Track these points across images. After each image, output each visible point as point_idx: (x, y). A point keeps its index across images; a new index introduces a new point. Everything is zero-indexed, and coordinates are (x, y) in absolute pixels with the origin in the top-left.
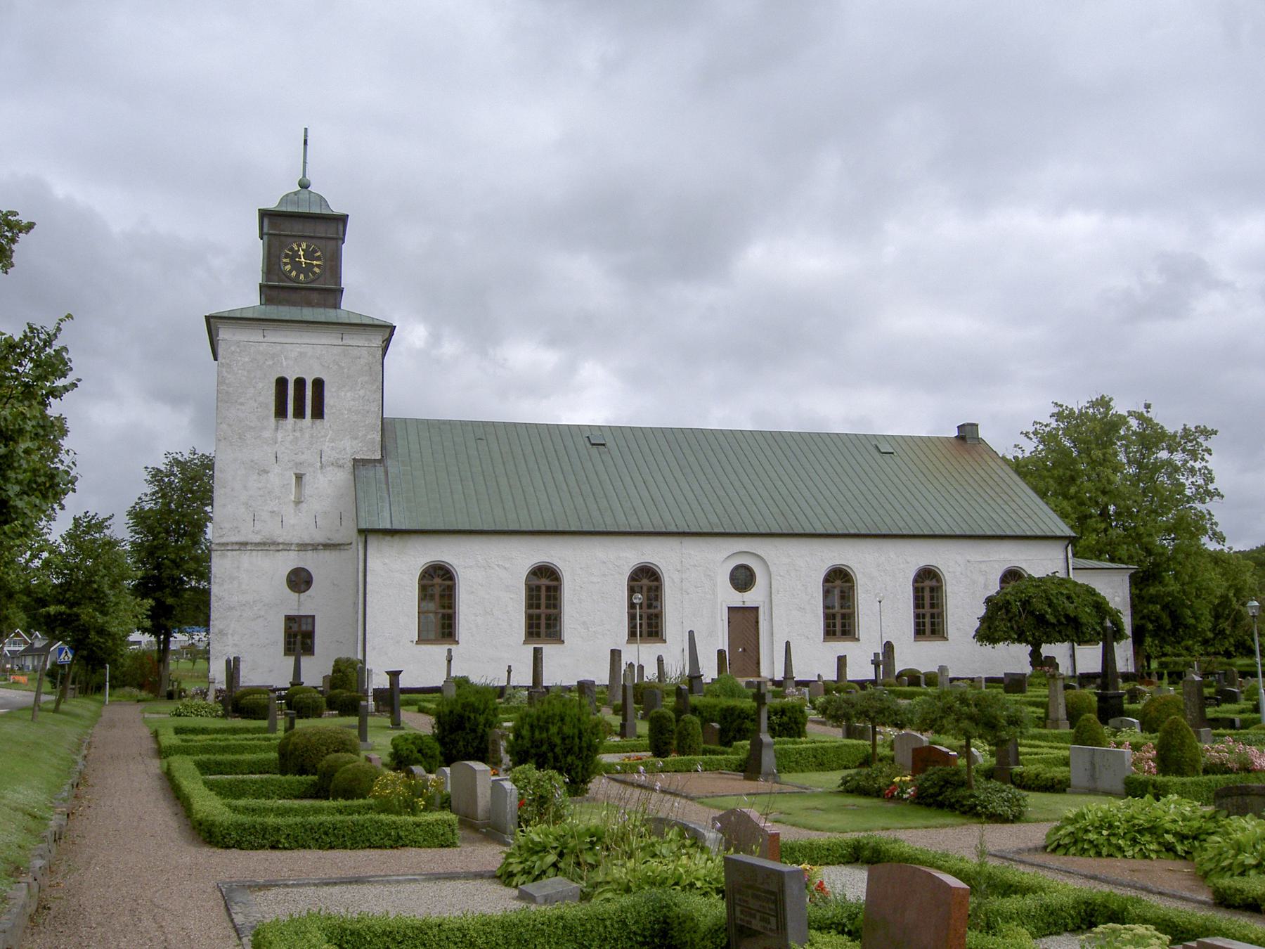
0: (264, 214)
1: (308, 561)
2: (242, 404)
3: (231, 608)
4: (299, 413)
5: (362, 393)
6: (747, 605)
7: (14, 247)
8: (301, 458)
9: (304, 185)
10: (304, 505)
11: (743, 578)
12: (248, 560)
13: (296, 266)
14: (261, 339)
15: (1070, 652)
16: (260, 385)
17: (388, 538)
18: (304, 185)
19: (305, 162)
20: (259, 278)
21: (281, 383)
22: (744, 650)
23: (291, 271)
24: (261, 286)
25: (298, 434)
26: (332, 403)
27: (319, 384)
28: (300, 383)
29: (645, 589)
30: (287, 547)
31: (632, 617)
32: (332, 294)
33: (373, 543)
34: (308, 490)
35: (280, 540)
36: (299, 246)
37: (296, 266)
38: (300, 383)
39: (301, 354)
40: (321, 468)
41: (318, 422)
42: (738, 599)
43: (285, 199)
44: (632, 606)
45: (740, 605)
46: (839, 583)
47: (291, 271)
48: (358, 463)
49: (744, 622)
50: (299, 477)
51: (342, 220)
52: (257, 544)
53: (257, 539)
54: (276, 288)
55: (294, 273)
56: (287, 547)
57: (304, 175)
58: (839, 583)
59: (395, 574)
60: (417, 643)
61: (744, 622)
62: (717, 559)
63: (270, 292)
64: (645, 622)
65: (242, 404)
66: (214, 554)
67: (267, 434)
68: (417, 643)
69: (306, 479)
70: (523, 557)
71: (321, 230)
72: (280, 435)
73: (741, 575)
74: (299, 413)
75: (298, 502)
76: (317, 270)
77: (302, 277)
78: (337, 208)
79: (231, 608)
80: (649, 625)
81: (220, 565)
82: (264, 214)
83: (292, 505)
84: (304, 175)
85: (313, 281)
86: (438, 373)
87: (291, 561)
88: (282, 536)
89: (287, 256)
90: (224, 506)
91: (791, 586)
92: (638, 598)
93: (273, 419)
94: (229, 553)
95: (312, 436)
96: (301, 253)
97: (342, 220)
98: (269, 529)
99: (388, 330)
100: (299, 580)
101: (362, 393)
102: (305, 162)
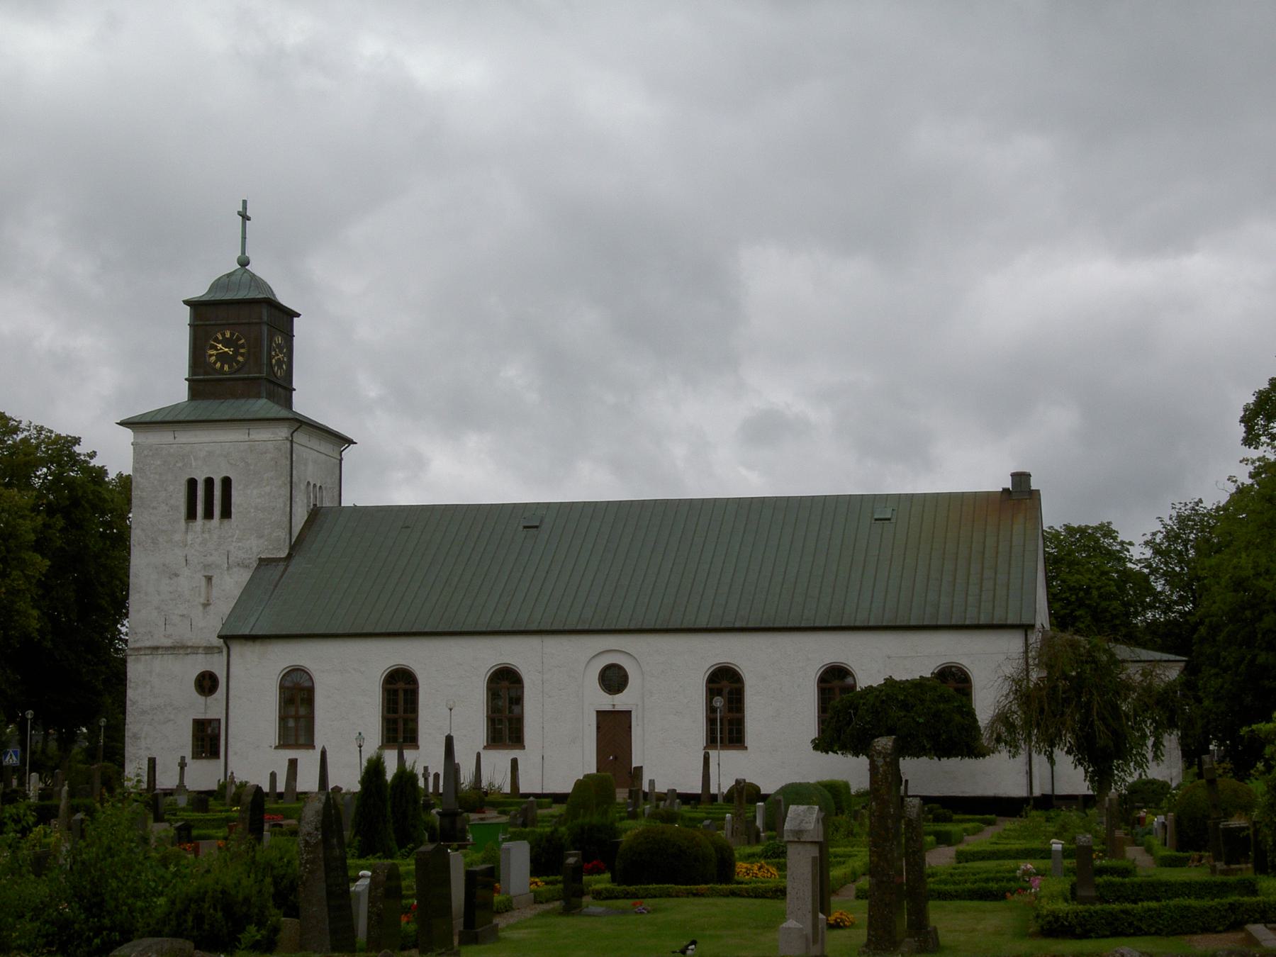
1: (216, 665)
2: (154, 508)
3: (144, 712)
4: (209, 514)
5: (268, 489)
6: (617, 708)
8: (210, 559)
10: (212, 607)
11: (613, 679)
12: (160, 664)
14: (246, 438)
15: (1025, 768)
16: (171, 488)
17: (250, 643)
19: (244, 238)
21: (192, 483)
22: (616, 758)
25: (206, 536)
27: (227, 482)
28: (209, 482)
29: (726, 691)
30: (194, 649)
31: (711, 722)
33: (237, 649)
34: (215, 592)
35: (190, 644)
38: (209, 482)
40: (228, 568)
41: (226, 521)
42: (608, 702)
43: (216, 286)
44: (711, 710)
45: (609, 708)
46: (725, 687)
48: (264, 563)
49: (614, 731)
50: (209, 579)
52: (167, 648)
53: (168, 643)
54: (205, 381)
56: (194, 649)
57: (243, 252)
58: (725, 687)
59: (255, 679)
60: (276, 748)
61: (614, 731)
62: (585, 655)
64: (726, 728)
65: (154, 508)
66: (129, 659)
67: (177, 537)
68: (276, 748)
69: (214, 580)
70: (385, 655)
72: (189, 537)
73: (207, 683)
74: (209, 514)
75: (206, 605)
77: (226, 367)
79: (144, 712)
80: (731, 731)
81: (135, 670)
83: (201, 608)
84: (243, 252)
85: (235, 372)
86: (421, 459)
87: (199, 664)
88: (192, 638)
90: (139, 611)
91: (666, 691)
92: (719, 702)
93: (183, 522)
94: (143, 658)
95: (220, 537)
98: (181, 632)
100: (207, 684)
101: (268, 489)
102: (244, 238)
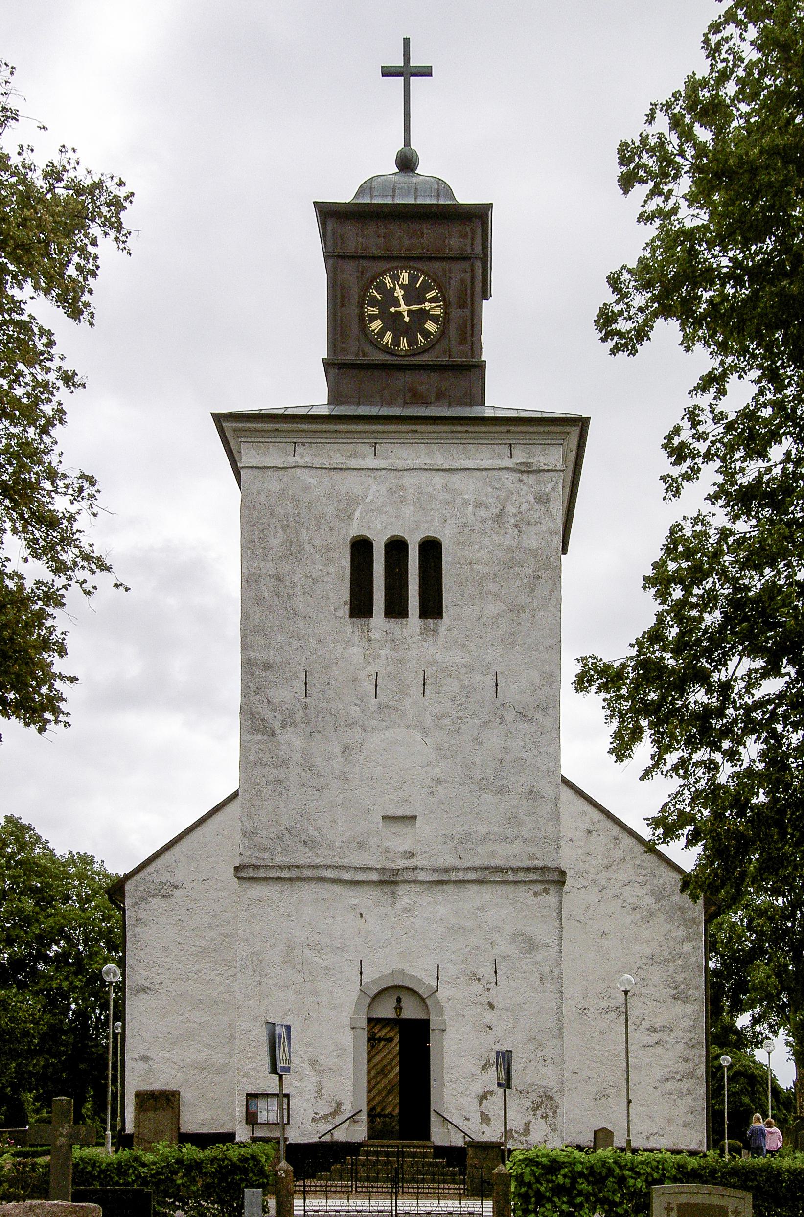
0: (329, 215)
7: (423, 169)
9: (406, 163)
13: (393, 322)
18: (406, 163)
20: (323, 352)
21: (361, 549)
23: (381, 333)
24: (328, 365)
26: (450, 559)
28: (396, 548)
32: (469, 371)
36: (395, 278)
37: (393, 322)
39: (399, 488)
47: (381, 333)
51: (478, 217)
55: (388, 337)
57: (407, 142)
63: (346, 367)
71: (429, 235)
76: (431, 326)
78: (464, 196)
82: (329, 215)
84: (407, 142)
89: (373, 302)
96: (399, 293)
97: (478, 217)
99: (575, 431)
